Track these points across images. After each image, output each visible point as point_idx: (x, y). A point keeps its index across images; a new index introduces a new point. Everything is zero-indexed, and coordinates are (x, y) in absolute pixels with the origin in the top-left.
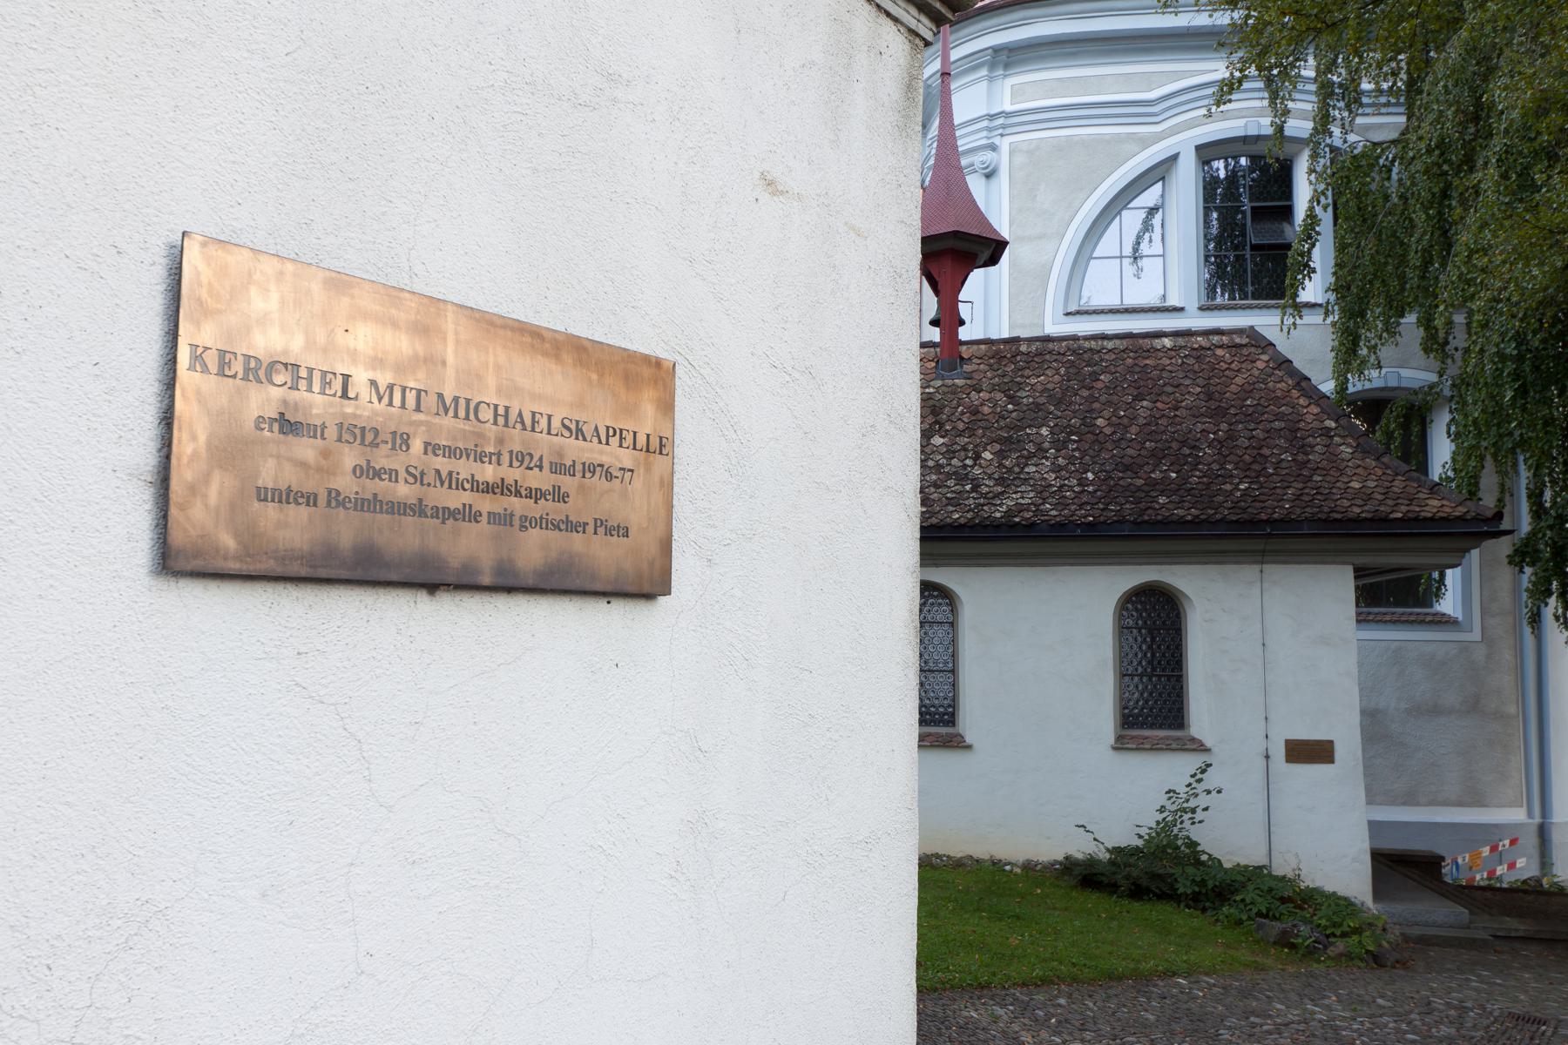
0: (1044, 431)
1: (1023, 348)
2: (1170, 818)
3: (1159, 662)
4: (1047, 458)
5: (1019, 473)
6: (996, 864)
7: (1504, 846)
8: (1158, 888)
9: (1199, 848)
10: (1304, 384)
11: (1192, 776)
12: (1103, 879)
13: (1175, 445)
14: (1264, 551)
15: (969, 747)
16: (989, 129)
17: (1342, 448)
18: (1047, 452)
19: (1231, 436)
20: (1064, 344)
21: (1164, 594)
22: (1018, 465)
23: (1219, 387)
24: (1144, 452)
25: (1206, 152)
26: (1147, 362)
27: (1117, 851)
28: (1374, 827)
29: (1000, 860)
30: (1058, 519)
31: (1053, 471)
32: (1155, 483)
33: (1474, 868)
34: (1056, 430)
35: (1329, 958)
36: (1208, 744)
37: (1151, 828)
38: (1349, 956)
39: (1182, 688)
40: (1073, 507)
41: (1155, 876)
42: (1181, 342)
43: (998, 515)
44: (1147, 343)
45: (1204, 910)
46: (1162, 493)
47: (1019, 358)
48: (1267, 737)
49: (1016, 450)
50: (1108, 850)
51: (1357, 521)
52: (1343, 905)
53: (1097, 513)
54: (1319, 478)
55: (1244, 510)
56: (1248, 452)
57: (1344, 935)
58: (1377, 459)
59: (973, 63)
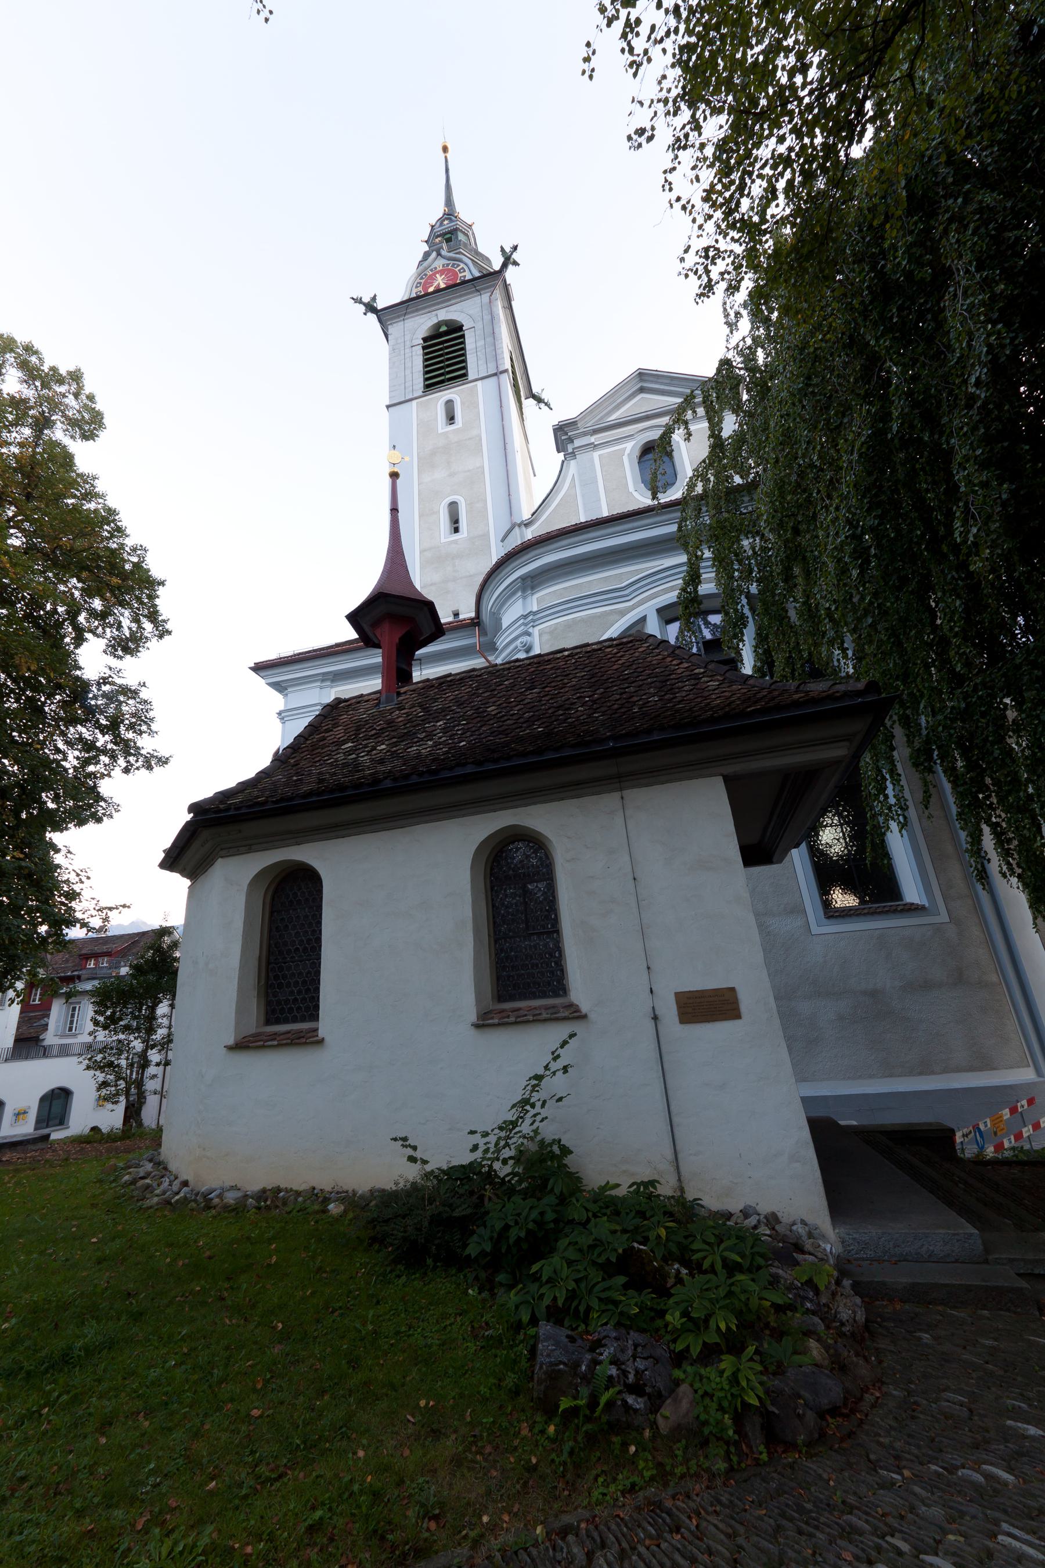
7: (1023, 1106)
16: (525, 625)
28: (805, 1100)
33: (999, 1134)
36: (584, 1008)
48: (652, 992)
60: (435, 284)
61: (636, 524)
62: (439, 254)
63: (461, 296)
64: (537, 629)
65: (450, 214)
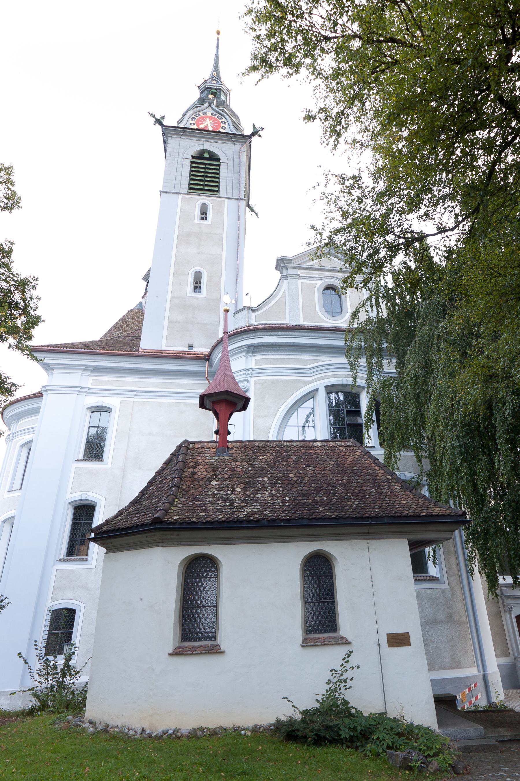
0: (266, 479)
1: (257, 444)
2: (333, 688)
3: (323, 594)
4: (267, 491)
5: (253, 497)
6: (236, 730)
8: (330, 736)
9: (350, 705)
10: (376, 461)
11: (344, 659)
12: (298, 733)
13: (325, 486)
14: (368, 533)
15: (223, 652)
16: (246, 374)
17: (396, 487)
18: (267, 488)
19: (349, 482)
20: (275, 443)
21: (324, 557)
22: (253, 494)
23: (342, 462)
24: (311, 488)
25: (330, 389)
26: (311, 451)
27: (305, 712)
29: (239, 727)
30: (272, 518)
31: (269, 497)
32: (317, 502)
34: (271, 478)
35: (431, 773)
36: (350, 639)
37: (323, 695)
38: (440, 770)
39: (335, 608)
40: (279, 512)
41: (328, 728)
42: (325, 444)
43: (242, 516)
44: (310, 444)
45: (357, 748)
46: (321, 506)
47: (254, 448)
49: (252, 487)
50: (300, 712)
51: (407, 517)
52: (426, 731)
53: (291, 514)
54: (388, 499)
55: (358, 512)
56: (357, 488)
57: (435, 755)
58: (410, 491)
59: (239, 350)
60: (205, 124)
61: (321, 335)
62: (210, 105)
63: (222, 140)
64: (253, 379)
65: (216, 77)
